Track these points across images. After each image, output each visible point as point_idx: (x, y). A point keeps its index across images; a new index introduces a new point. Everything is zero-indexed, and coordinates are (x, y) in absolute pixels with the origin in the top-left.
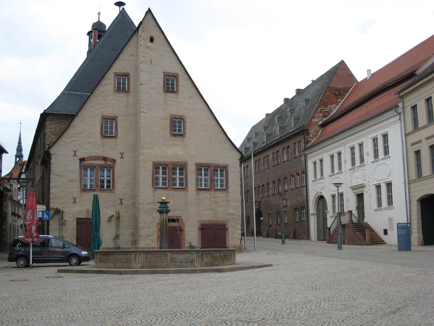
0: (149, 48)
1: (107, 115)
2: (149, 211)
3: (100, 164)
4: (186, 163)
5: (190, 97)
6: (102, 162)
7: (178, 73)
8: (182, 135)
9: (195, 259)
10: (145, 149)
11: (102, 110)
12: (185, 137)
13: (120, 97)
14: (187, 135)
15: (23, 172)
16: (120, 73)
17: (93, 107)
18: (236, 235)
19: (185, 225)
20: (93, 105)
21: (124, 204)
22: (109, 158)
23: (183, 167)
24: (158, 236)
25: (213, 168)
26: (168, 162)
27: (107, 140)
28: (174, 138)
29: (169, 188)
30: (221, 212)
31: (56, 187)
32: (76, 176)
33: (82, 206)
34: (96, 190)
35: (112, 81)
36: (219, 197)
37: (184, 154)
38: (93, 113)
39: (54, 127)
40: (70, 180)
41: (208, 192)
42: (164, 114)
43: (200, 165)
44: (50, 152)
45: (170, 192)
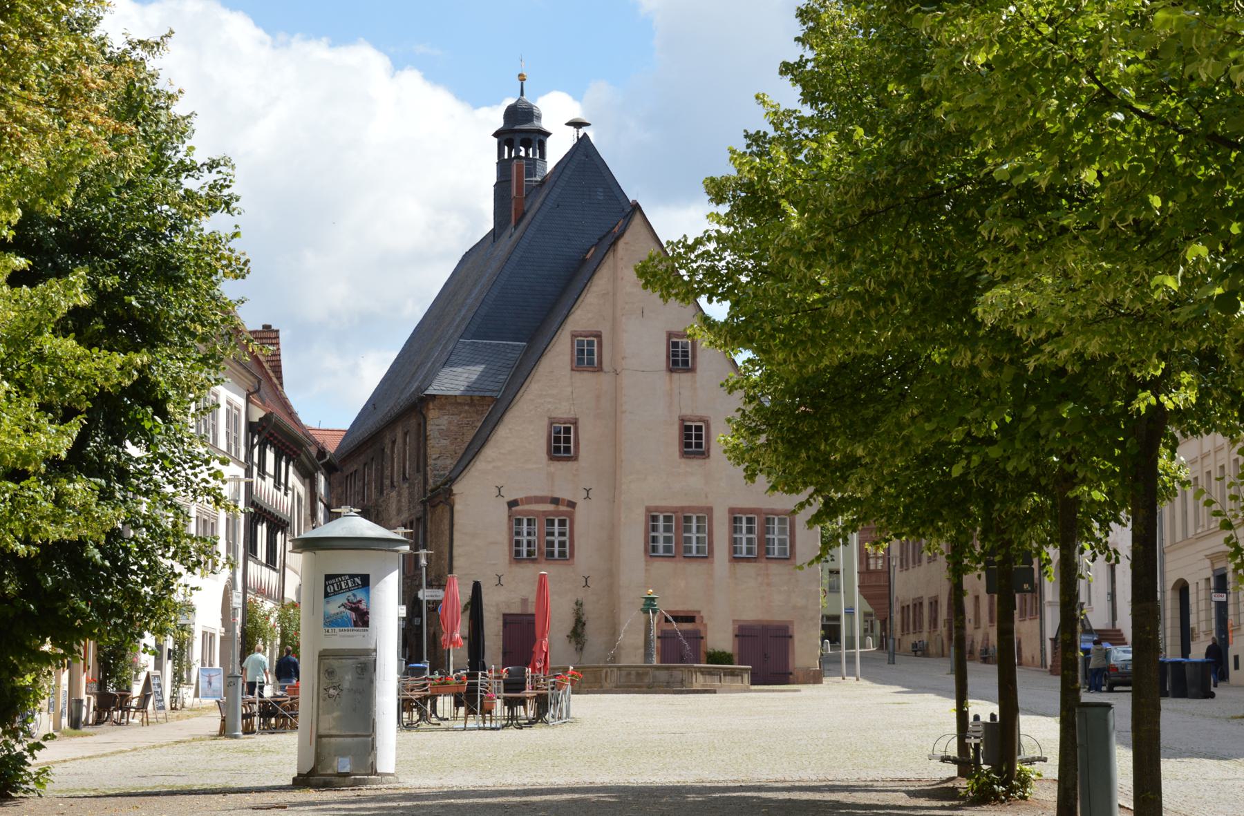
22: (563, 500)
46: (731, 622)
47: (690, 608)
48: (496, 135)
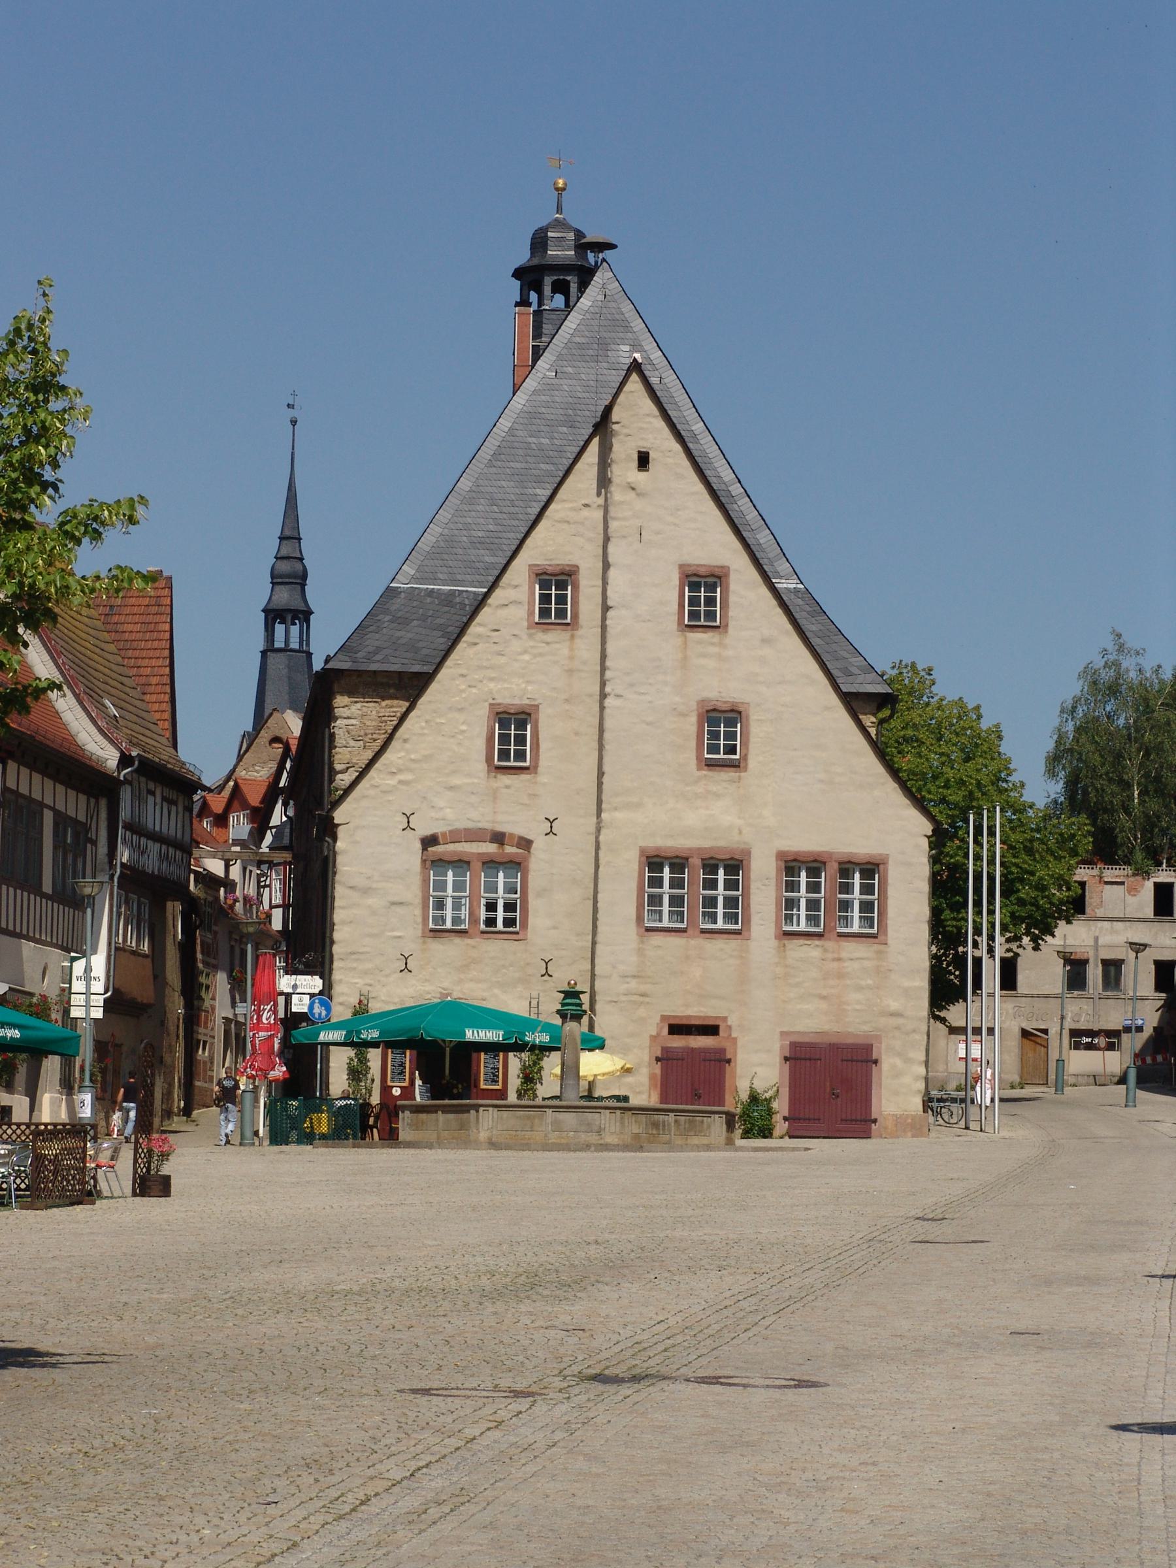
0: (633, 489)
1: (508, 701)
2: (623, 998)
3: (484, 854)
4: (748, 853)
5: (766, 641)
6: (491, 848)
7: (726, 564)
8: (735, 765)
9: (607, 1125)
10: (616, 809)
11: (492, 685)
12: (746, 771)
13: (548, 643)
14: (753, 762)
15: (281, 785)
16: (547, 567)
17: (463, 676)
18: (907, 1080)
19: (739, 1044)
20: (464, 672)
21: (555, 975)
22: (511, 835)
23: (735, 866)
24: (652, 1077)
25: (836, 866)
26: (690, 849)
27: (506, 779)
28: (710, 773)
29: (690, 931)
30: (857, 1007)
31: (351, 922)
32: (411, 891)
33: (426, 980)
34: (470, 931)
35: (522, 594)
36: (852, 960)
37: (739, 822)
38: (464, 695)
39: (360, 712)
40: (393, 903)
41: (817, 942)
42: (677, 699)
43: (792, 858)
44: (333, 818)
45: (693, 942)
46: (777, 1036)
47: (711, 1013)
48: (518, 273)
